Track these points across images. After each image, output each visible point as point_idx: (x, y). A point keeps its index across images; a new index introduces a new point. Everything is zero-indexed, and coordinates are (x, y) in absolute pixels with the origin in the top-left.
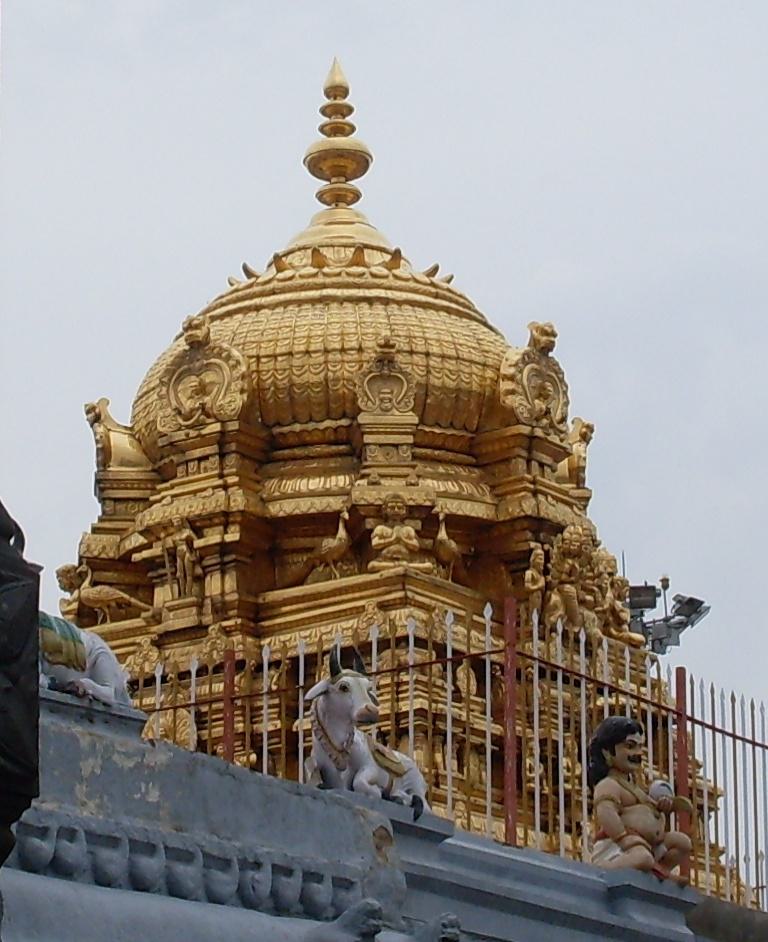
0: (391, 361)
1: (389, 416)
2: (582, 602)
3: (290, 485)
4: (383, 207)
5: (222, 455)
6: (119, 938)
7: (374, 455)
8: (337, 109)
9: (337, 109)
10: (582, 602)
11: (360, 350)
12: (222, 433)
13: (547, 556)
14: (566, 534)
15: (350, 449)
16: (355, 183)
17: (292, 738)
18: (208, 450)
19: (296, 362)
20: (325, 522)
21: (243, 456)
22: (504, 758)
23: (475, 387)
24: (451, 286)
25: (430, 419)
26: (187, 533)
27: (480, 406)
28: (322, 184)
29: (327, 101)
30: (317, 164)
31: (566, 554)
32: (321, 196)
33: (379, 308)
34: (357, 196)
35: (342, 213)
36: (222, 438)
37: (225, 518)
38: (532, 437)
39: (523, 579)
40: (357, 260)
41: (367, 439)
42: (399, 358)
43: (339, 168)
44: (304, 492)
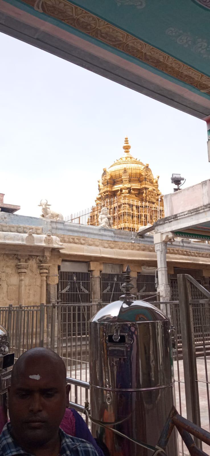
1: (125, 177)
5: (108, 184)
6: (10, 214)
7: (124, 182)
8: (126, 141)
9: (126, 141)
10: (152, 197)
12: (107, 181)
13: (146, 192)
14: (149, 189)
18: (106, 184)
19: (116, 172)
21: (110, 184)
22: (139, 217)
23: (138, 172)
26: (103, 194)
27: (139, 174)
28: (125, 150)
31: (149, 192)
32: (125, 152)
33: (133, 164)
37: (107, 191)
38: (145, 178)
39: (143, 195)
41: (123, 180)
42: (127, 170)
43: (127, 148)
44: (117, 187)
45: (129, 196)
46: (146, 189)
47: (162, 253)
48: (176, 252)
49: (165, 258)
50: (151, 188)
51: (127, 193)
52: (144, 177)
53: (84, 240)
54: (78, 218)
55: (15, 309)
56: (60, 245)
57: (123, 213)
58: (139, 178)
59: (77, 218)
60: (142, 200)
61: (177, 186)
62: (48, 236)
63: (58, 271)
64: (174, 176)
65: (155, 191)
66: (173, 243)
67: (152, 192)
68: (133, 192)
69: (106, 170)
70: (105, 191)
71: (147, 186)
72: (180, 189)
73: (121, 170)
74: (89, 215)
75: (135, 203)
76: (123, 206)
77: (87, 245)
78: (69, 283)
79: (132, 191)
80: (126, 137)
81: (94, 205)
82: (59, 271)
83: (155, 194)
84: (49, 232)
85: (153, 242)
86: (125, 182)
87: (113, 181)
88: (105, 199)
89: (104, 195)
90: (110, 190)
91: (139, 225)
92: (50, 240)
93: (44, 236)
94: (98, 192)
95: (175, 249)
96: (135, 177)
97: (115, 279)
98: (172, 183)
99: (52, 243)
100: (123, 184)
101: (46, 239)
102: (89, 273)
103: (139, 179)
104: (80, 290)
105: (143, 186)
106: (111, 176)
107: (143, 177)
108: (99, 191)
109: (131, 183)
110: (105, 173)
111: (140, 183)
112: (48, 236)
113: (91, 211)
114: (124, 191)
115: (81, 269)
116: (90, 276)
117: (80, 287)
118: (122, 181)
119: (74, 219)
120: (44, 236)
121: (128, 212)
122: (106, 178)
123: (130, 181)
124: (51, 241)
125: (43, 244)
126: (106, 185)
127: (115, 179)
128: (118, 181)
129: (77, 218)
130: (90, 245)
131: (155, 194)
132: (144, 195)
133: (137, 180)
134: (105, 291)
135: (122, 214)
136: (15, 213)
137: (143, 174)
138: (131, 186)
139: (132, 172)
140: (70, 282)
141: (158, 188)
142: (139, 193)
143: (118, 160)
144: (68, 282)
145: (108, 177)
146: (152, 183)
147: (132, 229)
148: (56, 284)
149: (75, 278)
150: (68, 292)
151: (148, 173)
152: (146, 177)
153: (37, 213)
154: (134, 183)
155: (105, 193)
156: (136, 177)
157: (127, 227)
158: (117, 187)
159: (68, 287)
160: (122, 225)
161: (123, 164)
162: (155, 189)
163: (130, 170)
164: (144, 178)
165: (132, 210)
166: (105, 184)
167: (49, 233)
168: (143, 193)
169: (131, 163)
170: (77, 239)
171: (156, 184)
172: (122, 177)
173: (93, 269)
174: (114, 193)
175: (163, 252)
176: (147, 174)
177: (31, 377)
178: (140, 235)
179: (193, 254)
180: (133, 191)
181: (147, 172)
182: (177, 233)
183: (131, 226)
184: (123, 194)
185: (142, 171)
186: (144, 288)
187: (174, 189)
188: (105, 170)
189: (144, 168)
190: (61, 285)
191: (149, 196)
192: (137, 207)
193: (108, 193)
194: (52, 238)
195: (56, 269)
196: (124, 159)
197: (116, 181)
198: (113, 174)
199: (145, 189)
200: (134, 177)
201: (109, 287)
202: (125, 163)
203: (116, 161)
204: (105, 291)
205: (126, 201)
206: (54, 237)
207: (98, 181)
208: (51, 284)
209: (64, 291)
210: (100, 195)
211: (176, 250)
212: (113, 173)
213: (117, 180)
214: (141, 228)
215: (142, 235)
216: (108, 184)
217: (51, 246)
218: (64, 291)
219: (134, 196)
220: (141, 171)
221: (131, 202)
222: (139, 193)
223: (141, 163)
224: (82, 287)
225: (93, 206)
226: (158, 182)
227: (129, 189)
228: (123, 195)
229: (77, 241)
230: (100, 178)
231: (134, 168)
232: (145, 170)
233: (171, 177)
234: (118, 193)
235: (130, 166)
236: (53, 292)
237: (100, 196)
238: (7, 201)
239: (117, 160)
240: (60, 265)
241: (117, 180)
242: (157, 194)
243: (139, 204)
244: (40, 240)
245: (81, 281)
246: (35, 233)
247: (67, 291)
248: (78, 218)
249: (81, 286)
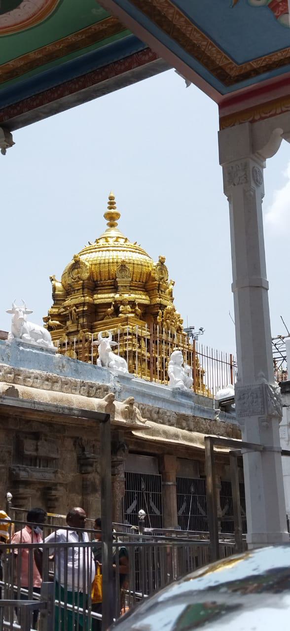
5: (83, 289)
7: (121, 289)
8: (112, 204)
9: (112, 204)
12: (83, 283)
18: (80, 288)
21: (88, 289)
26: (74, 308)
32: (108, 224)
37: (84, 304)
43: (112, 219)
52: (158, 282)
80: (112, 195)
86: (122, 289)
87: (94, 284)
89: (77, 310)
96: (138, 281)
103: (144, 287)
121: (139, 353)
127: (99, 279)
128: (104, 284)
133: (140, 286)
142: (148, 313)
156: (139, 282)
164: (157, 285)
168: (157, 314)
181: (162, 274)
197: (100, 285)
200: (136, 281)
203: (88, 246)
207: (51, 278)
213: (102, 282)
221: (138, 332)
225: (34, 330)
232: (159, 269)
239: (136, 243)
241: (102, 282)
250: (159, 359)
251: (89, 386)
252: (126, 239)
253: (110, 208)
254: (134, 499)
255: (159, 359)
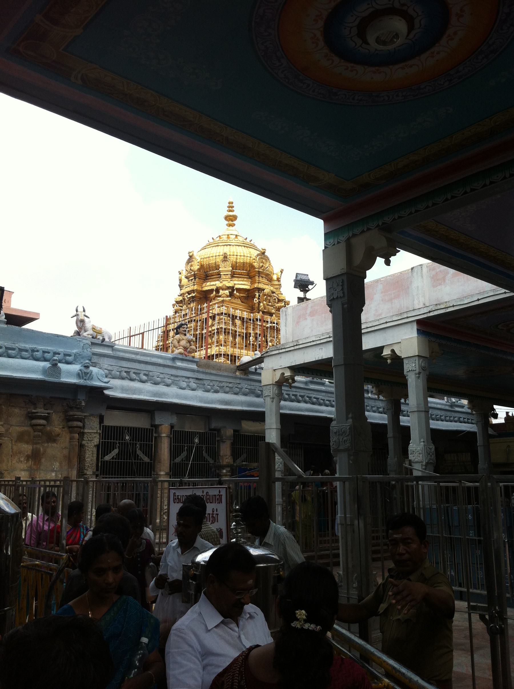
0: (226, 257)
1: (225, 268)
2: (268, 305)
3: (208, 284)
4: (240, 228)
5: (195, 279)
8: (231, 207)
9: (231, 207)
10: (268, 305)
11: (251, 257)
12: (194, 274)
13: (259, 296)
15: (218, 276)
16: (234, 222)
17: (202, 334)
20: (211, 291)
21: (199, 279)
24: (252, 242)
25: (234, 268)
26: (187, 294)
28: (227, 222)
29: (228, 205)
30: (227, 218)
31: (265, 295)
32: (227, 225)
34: (234, 225)
35: (231, 228)
36: (195, 275)
37: (193, 291)
38: (259, 271)
40: (228, 238)
43: (231, 219)
44: (209, 286)
45: (229, 301)
46: (260, 290)
47: (273, 401)
48: (300, 398)
49: (279, 407)
50: (268, 289)
51: (227, 296)
53: (145, 375)
54: (141, 334)
55: (24, 483)
56: (105, 383)
57: (218, 329)
58: (249, 271)
59: (139, 334)
60: (252, 309)
61: (302, 293)
62: (85, 366)
63: (98, 426)
64: (298, 278)
65: (274, 294)
66: (293, 385)
67: (270, 296)
68: (238, 294)
69: (193, 255)
70: (191, 291)
71: (261, 286)
72: (308, 300)
73: (219, 256)
74: (160, 331)
75: (238, 313)
76: (217, 318)
77: (151, 383)
78: (118, 445)
79: (235, 292)
81: (170, 312)
82: (102, 424)
83: (275, 299)
84: (87, 361)
85: (260, 381)
88: (189, 304)
90: (198, 289)
91: (244, 352)
92: (88, 373)
93: (76, 368)
94: (178, 291)
95: (298, 394)
97: (197, 441)
98: (295, 287)
99: (91, 378)
100: (221, 280)
101: (82, 373)
102: (152, 430)
104: (137, 457)
105: (256, 285)
106: (201, 265)
107: (256, 270)
108: (181, 289)
109: (234, 279)
110: (191, 258)
111: (250, 280)
112: (85, 366)
113: (162, 323)
114: (221, 292)
115: (138, 422)
116: (154, 435)
117: (136, 451)
118: (221, 275)
119: (135, 335)
120: (76, 368)
122: (192, 268)
123: (233, 275)
124: (88, 375)
125: (73, 380)
126: (192, 280)
127: (208, 270)
129: (139, 334)
130: (156, 383)
131: (275, 299)
132: (256, 300)
134: (178, 460)
135: (216, 331)
136: (28, 326)
137: (255, 264)
138: (235, 284)
139: (238, 261)
140: (119, 443)
141: (281, 290)
143: (215, 238)
144: (116, 444)
145: (196, 267)
146: (270, 280)
147: (231, 356)
148: (95, 446)
149: (127, 438)
150: (116, 459)
151: (263, 263)
152: (260, 270)
153: (68, 329)
154: (240, 279)
155: (189, 294)
157: (222, 353)
158: (209, 286)
159: (116, 451)
160: (214, 350)
161: (224, 245)
162: (274, 290)
163: (235, 257)
165: (234, 324)
166: (191, 279)
167: (88, 363)
168: (254, 297)
169: (236, 245)
170: (134, 373)
171: (277, 283)
172: (220, 268)
173: (159, 423)
174: (206, 295)
175: (275, 400)
176: (262, 266)
177: (487, 605)
178: (241, 370)
179: (327, 402)
180: (237, 292)
181: (262, 262)
182: (297, 369)
183: (230, 351)
184: (220, 296)
185: (254, 259)
186: (244, 456)
187: (298, 298)
188: (191, 254)
189: (258, 255)
190: (103, 448)
191: (264, 302)
192: (242, 319)
193: (195, 293)
194: (92, 372)
195: (96, 421)
196: (225, 238)
198: (205, 262)
199: (259, 291)
201: (184, 454)
202: (227, 245)
203: (211, 241)
204: (178, 460)
205: (224, 309)
206: (94, 370)
208: (86, 444)
209: (107, 458)
210: (181, 295)
211: (300, 396)
212: (205, 260)
214: (246, 357)
215: (245, 368)
216: (195, 279)
217: (90, 383)
218: (107, 458)
219: (239, 302)
220: (252, 259)
221: (232, 311)
222: (248, 296)
223: (254, 246)
224: (139, 452)
226: (282, 280)
227: (232, 289)
228: (220, 298)
229: (134, 376)
230: (182, 266)
231: (242, 254)
232: (259, 259)
233: (295, 278)
234: (212, 295)
235: (235, 251)
236: (90, 456)
237: (181, 298)
238: (16, 304)
240: (103, 414)
242: (278, 299)
243: (245, 315)
244: (69, 374)
245: (138, 441)
246: (64, 361)
247: (113, 458)
248: (141, 335)
249: (137, 449)
250: (252, 334)
251: (64, 354)
252: (236, 236)
253: (230, 211)
254: (116, 448)
255: (252, 334)
